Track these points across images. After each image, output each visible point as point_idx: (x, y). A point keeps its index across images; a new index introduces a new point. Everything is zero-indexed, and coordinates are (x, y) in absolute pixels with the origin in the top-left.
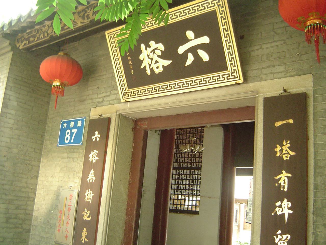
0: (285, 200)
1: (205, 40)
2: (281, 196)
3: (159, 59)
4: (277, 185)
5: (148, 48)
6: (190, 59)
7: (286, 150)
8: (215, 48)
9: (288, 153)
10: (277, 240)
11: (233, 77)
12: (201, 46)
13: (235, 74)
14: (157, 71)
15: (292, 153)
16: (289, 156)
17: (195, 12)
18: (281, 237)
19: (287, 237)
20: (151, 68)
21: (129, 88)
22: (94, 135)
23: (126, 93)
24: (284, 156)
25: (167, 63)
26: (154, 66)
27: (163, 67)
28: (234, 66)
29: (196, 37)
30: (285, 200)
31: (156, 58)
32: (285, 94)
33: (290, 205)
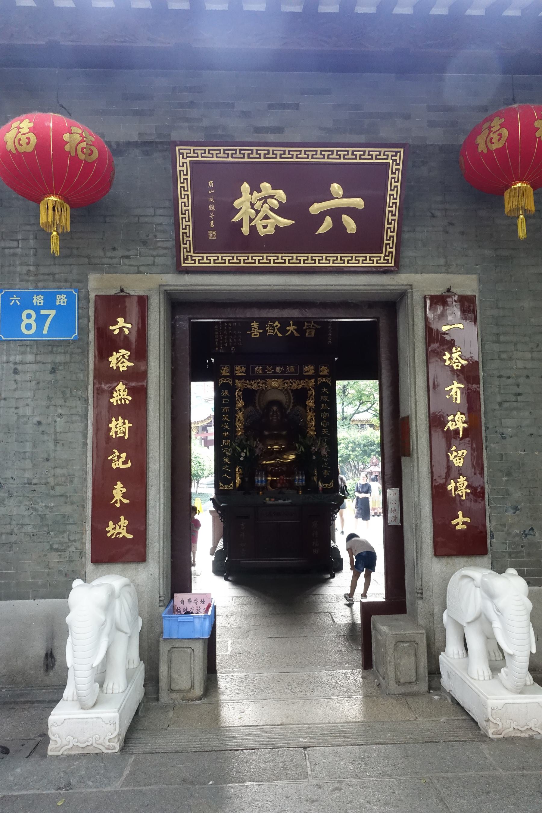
1: (358, 202)
4: (447, 397)
5: (255, 192)
6: (327, 224)
7: (457, 359)
9: (459, 362)
10: (452, 458)
11: (386, 261)
12: (351, 211)
13: (390, 258)
14: (262, 232)
16: (460, 365)
18: (456, 454)
19: (463, 453)
22: (116, 323)
23: (189, 257)
24: (455, 365)
26: (259, 223)
27: (277, 227)
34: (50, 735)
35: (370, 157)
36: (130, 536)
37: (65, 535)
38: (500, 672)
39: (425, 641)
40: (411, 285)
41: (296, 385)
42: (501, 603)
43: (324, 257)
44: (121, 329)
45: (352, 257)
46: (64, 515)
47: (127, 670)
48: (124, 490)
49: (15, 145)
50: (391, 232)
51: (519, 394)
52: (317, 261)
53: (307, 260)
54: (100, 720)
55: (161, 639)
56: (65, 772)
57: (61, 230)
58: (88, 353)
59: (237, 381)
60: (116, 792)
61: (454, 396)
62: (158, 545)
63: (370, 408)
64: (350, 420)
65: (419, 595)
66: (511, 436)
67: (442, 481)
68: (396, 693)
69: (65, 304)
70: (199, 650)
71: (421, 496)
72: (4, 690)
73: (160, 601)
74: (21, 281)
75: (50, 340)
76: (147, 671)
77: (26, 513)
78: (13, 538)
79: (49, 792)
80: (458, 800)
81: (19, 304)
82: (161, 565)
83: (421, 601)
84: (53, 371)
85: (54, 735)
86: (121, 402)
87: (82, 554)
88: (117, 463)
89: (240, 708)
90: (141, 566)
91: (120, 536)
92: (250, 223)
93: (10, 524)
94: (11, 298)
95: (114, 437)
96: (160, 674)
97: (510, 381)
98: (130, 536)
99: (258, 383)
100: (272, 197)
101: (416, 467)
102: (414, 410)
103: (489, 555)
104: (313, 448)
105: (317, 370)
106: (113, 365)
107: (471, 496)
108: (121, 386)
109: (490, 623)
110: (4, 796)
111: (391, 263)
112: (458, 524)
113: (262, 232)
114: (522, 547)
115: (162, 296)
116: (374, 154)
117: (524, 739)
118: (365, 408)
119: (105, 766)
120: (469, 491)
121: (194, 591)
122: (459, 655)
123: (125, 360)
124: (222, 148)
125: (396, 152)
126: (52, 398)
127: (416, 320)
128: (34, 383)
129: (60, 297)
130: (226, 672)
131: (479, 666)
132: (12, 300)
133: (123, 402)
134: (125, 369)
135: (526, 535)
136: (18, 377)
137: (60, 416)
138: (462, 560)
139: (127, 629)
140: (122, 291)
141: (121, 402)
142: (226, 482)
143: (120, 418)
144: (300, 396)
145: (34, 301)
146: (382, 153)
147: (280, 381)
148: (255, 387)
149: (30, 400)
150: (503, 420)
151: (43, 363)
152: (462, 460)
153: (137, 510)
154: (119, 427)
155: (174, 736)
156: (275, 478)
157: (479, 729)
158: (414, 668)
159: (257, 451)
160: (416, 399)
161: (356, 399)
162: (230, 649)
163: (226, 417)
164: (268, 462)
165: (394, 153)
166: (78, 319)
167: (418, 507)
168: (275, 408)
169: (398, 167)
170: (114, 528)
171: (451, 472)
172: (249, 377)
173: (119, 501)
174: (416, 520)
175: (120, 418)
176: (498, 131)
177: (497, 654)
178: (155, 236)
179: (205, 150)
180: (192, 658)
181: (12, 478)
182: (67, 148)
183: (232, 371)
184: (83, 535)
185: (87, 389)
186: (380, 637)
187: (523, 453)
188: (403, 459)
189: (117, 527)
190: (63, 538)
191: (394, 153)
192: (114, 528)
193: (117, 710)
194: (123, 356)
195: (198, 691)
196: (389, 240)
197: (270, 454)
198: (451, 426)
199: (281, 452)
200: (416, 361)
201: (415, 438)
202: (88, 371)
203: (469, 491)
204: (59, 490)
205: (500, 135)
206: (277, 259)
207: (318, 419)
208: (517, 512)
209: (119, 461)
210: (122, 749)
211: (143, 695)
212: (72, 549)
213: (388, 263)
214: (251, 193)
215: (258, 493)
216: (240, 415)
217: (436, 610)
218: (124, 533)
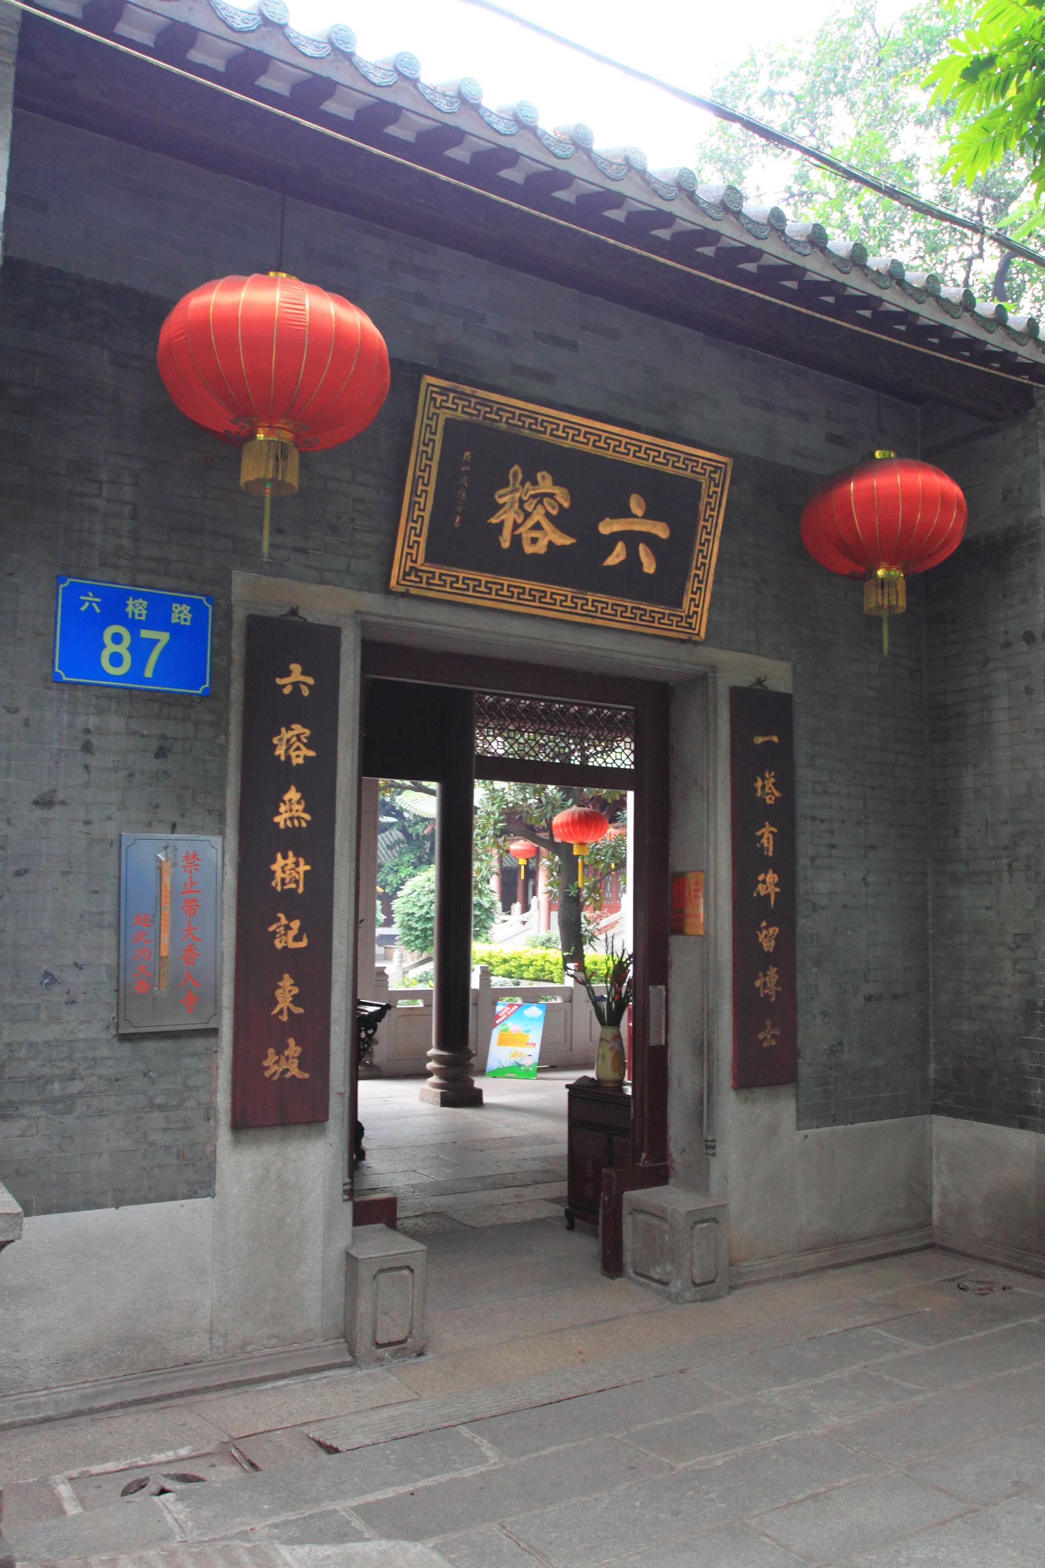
0: (771, 871)
1: (661, 531)
2: (765, 961)
3: (546, 524)
5: (528, 485)
6: (617, 555)
8: (676, 555)
9: (772, 794)
12: (650, 539)
14: (529, 549)
17: (667, 464)
20: (517, 532)
21: (428, 559)
22: (288, 673)
24: (767, 798)
25: (563, 540)
27: (551, 544)
28: (697, 606)
29: (647, 516)
30: (771, 871)
31: (538, 516)
32: (758, 687)
33: (777, 879)
44: (296, 685)
48: (296, 991)
51: (834, 846)
52: (471, 587)
58: (228, 724)
61: (766, 845)
69: (188, 623)
74: (103, 565)
78: (76, 1087)
81: (98, 611)
84: (161, 753)
86: (293, 824)
87: (209, 1112)
91: (288, 1075)
94: (82, 598)
95: (279, 888)
106: (280, 752)
108: (293, 795)
113: (529, 549)
123: (302, 746)
128: (123, 773)
129: (179, 609)
132: (84, 602)
133: (296, 823)
134: (300, 761)
141: (293, 824)
143: (290, 854)
145: (129, 609)
149: (115, 807)
166: (212, 656)
175: (290, 854)
178: (352, 520)
189: (283, 1060)
192: (277, 1062)
194: (298, 736)
208: (827, 1019)
212: (191, 1103)
218: (294, 1070)
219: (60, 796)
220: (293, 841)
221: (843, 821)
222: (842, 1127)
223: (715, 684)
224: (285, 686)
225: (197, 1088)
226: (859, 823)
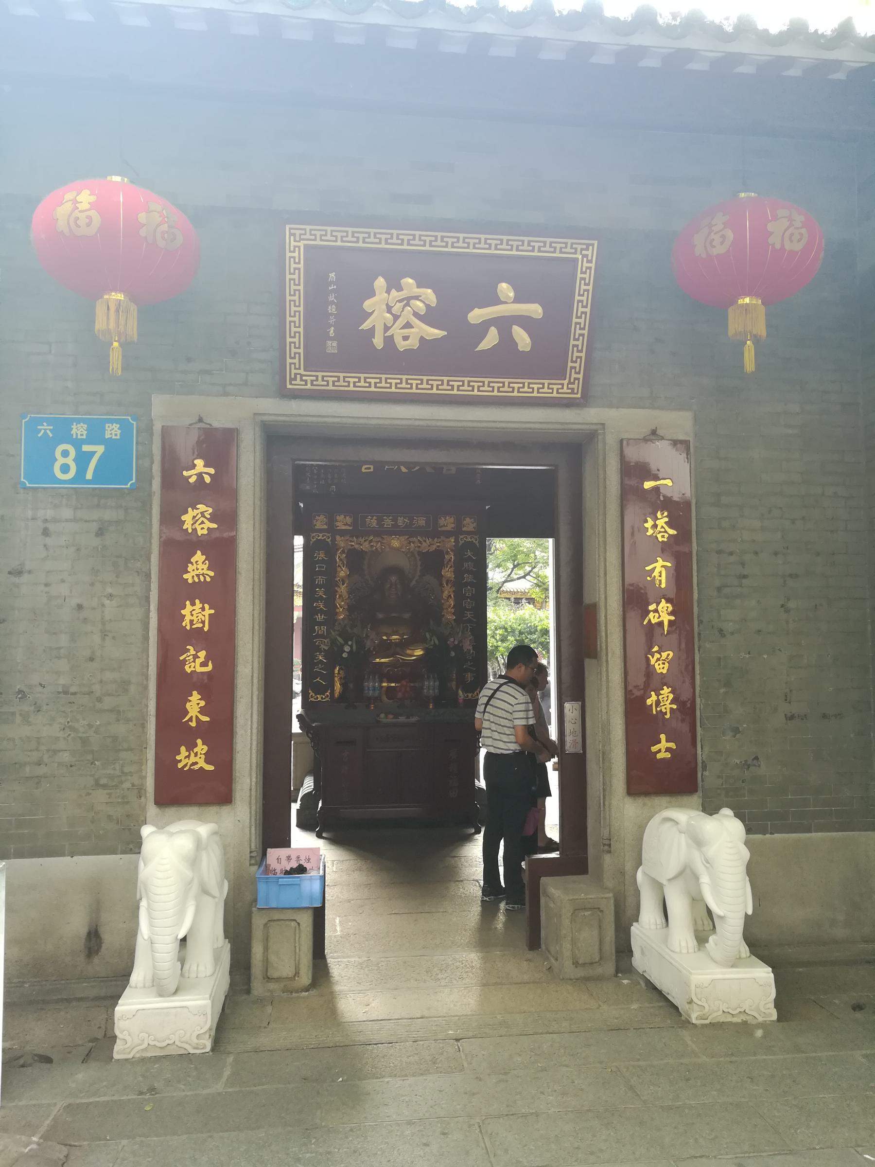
2: (190, 737)
4: (649, 578)
5: (393, 290)
6: (491, 339)
9: (666, 532)
12: (525, 322)
14: (402, 345)
15: (672, 532)
16: (666, 535)
18: (659, 656)
19: (669, 655)
22: (194, 466)
23: (298, 376)
24: (659, 536)
25: (435, 333)
26: (397, 332)
27: (422, 339)
29: (516, 300)
34: (117, 1032)
35: (552, 250)
36: (211, 768)
37: (117, 766)
38: (707, 941)
39: (613, 908)
40: (603, 424)
41: (428, 545)
42: (711, 851)
43: (486, 383)
45: (524, 384)
46: (115, 738)
47: (214, 950)
48: (203, 703)
49: (68, 223)
50: (578, 351)
53: (463, 385)
54: (186, 1010)
55: (254, 909)
56: (143, 1076)
57: (123, 339)
58: (151, 509)
59: (338, 537)
60: (219, 1094)
62: (248, 780)
63: (528, 574)
64: (498, 591)
65: (606, 847)
66: (732, 634)
67: (638, 693)
68: (572, 977)
70: (306, 921)
71: (611, 713)
72: (27, 985)
73: (251, 857)
75: (96, 489)
76: (234, 953)
77: (61, 734)
79: (129, 1097)
80: (652, 1088)
82: (254, 808)
83: (609, 855)
84: (100, 533)
85: (122, 1032)
86: (199, 579)
87: (140, 792)
88: (193, 664)
89: (361, 998)
90: (225, 810)
91: (196, 767)
92: (385, 333)
93: (37, 750)
95: (188, 628)
96: (253, 956)
97: (732, 559)
98: (211, 768)
99: (371, 541)
100: (417, 298)
101: (604, 674)
102: (603, 597)
103: (700, 793)
104: (452, 640)
105: (459, 524)
106: (188, 526)
107: (678, 714)
108: (199, 557)
109: (697, 878)
110: (70, 1104)
111: (577, 393)
112: (660, 751)
113: (402, 345)
114: (743, 782)
115: (257, 429)
116: (558, 246)
117: (736, 1024)
118: (521, 573)
119: (196, 1068)
120: (675, 707)
121: (292, 846)
122: (656, 924)
123: (205, 521)
124: (350, 230)
125: (588, 245)
126: (98, 570)
127: (608, 472)
130: (338, 957)
131: (681, 934)
134: (205, 532)
135: (749, 766)
136: (49, 541)
137: (110, 596)
138: (664, 800)
139: (215, 891)
140: (200, 420)
141: (199, 579)
142: (319, 690)
143: (197, 601)
144: (432, 562)
145: (73, 432)
146: (569, 245)
147: (403, 538)
148: (365, 547)
150: (722, 612)
151: (86, 521)
152: (667, 665)
153: (219, 732)
154: (196, 614)
155: (280, 1033)
156: (393, 685)
157: (680, 1014)
158: (598, 943)
159: (368, 644)
160: (606, 581)
161: (508, 560)
162: (338, 928)
163: (320, 592)
164: (383, 660)
165: (585, 247)
167: (606, 728)
168: (394, 578)
169: (589, 265)
170: (188, 757)
171: (652, 682)
172: (357, 531)
173: (194, 719)
174: (603, 746)
175: (197, 601)
176: (721, 231)
177: (706, 923)
179: (326, 231)
180: (297, 935)
181: (41, 685)
182: (143, 232)
183: (331, 522)
184: (142, 765)
185: (149, 559)
186: (552, 905)
187: (747, 656)
188: (588, 662)
190: (114, 769)
191: (585, 247)
192: (188, 757)
193: (208, 996)
194: (202, 514)
195: (305, 978)
196: (576, 362)
197: (386, 648)
198: (653, 618)
199: (403, 645)
200: (608, 530)
201: (603, 634)
202: (151, 534)
203: (675, 707)
204: (108, 702)
205: (723, 237)
206: (422, 384)
207: (459, 597)
208: (738, 736)
209: (196, 662)
210: (213, 1049)
211: (228, 986)
212: (127, 785)
213: (573, 393)
214: (388, 292)
215: (368, 707)
216: (343, 589)
217: (629, 866)
218: (202, 764)
219: (27, 567)
220: (197, 591)
221: (756, 553)
222: (760, 836)
223: (604, 439)
224: (190, 477)
225: (131, 774)
226: (776, 554)
